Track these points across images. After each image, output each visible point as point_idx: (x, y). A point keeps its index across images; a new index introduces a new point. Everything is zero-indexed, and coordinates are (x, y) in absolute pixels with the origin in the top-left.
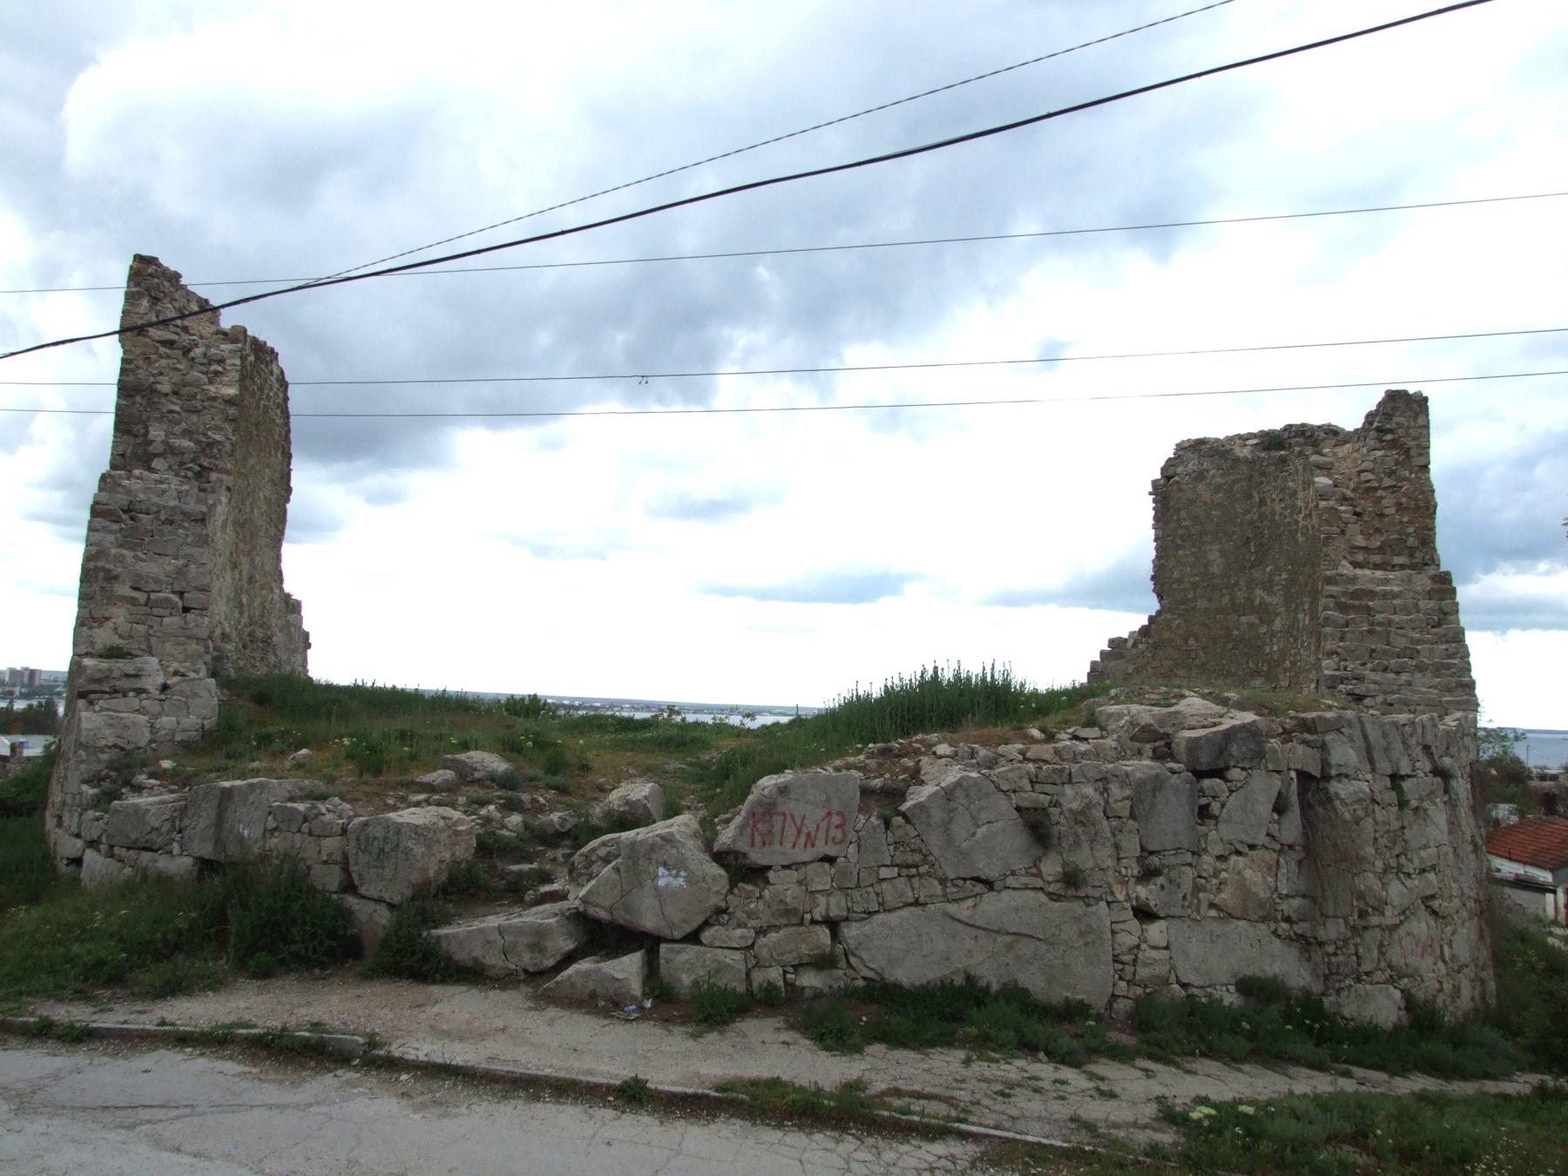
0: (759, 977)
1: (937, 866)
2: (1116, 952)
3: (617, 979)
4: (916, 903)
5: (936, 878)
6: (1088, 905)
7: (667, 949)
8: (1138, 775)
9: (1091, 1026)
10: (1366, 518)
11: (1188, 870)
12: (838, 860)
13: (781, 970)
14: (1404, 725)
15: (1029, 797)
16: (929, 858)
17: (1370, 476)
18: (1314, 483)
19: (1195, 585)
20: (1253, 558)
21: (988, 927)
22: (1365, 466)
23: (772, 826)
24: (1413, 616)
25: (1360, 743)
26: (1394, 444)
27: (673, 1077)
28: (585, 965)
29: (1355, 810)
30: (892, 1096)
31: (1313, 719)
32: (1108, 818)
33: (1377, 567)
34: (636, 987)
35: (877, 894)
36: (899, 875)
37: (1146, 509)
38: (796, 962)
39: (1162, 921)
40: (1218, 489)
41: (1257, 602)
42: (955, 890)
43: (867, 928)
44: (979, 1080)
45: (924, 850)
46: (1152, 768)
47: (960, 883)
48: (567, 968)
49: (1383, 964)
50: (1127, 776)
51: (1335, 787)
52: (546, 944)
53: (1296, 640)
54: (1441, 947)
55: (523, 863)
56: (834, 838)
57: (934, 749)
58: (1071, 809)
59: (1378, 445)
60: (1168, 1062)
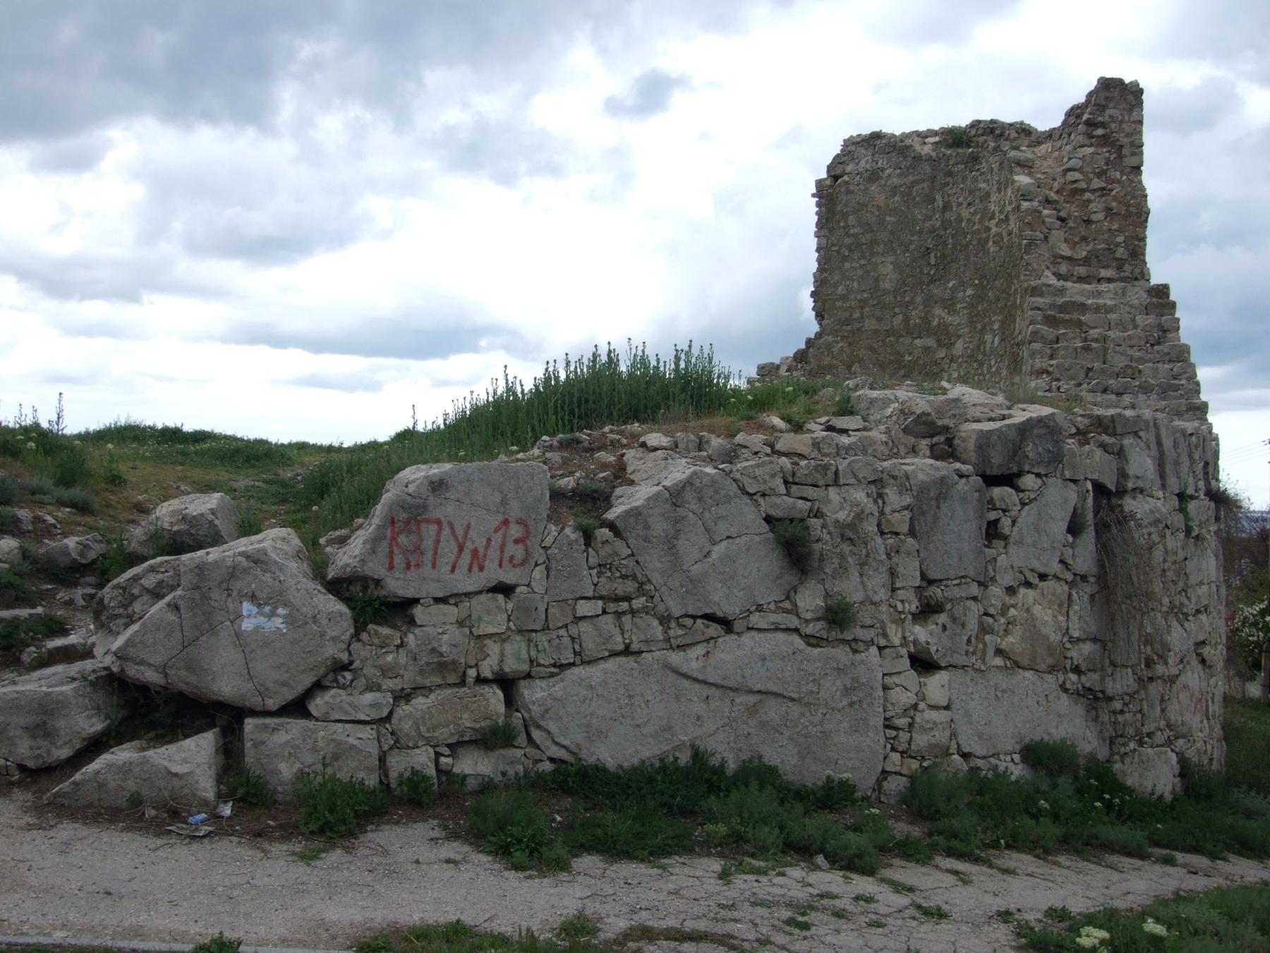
0: (399, 764)
1: (657, 599)
2: (889, 714)
3: (176, 775)
4: (627, 651)
5: (655, 616)
6: (855, 651)
7: (256, 726)
8: (921, 477)
9: (874, 815)
10: (1071, 224)
11: (971, 603)
12: (518, 590)
13: (431, 751)
14: (1191, 435)
15: (783, 504)
16: (648, 587)
17: (1077, 176)
18: (1013, 181)
19: (863, 304)
20: (932, 272)
21: (723, 683)
22: (1072, 163)
23: (421, 540)
24: (1130, 333)
25: (1154, 452)
26: (1105, 140)
27: (282, 931)
28: (123, 754)
29: (1150, 534)
30: (639, 939)
31: (1112, 416)
32: (882, 533)
33: (1081, 279)
34: (206, 786)
35: (573, 639)
36: (604, 612)
37: (807, 211)
38: (452, 740)
39: (943, 672)
40: (894, 190)
41: (935, 323)
42: (680, 632)
43: (558, 688)
44: (754, 904)
45: (639, 576)
46: (938, 469)
47: (688, 622)
48: (92, 761)
49: (1162, 724)
50: (908, 478)
51: (1129, 504)
52: (57, 726)
53: (981, 365)
54: (1207, 701)
55: (19, 607)
56: (512, 558)
57: (642, 439)
58: (837, 521)
59: (1087, 142)
60: (976, 860)
